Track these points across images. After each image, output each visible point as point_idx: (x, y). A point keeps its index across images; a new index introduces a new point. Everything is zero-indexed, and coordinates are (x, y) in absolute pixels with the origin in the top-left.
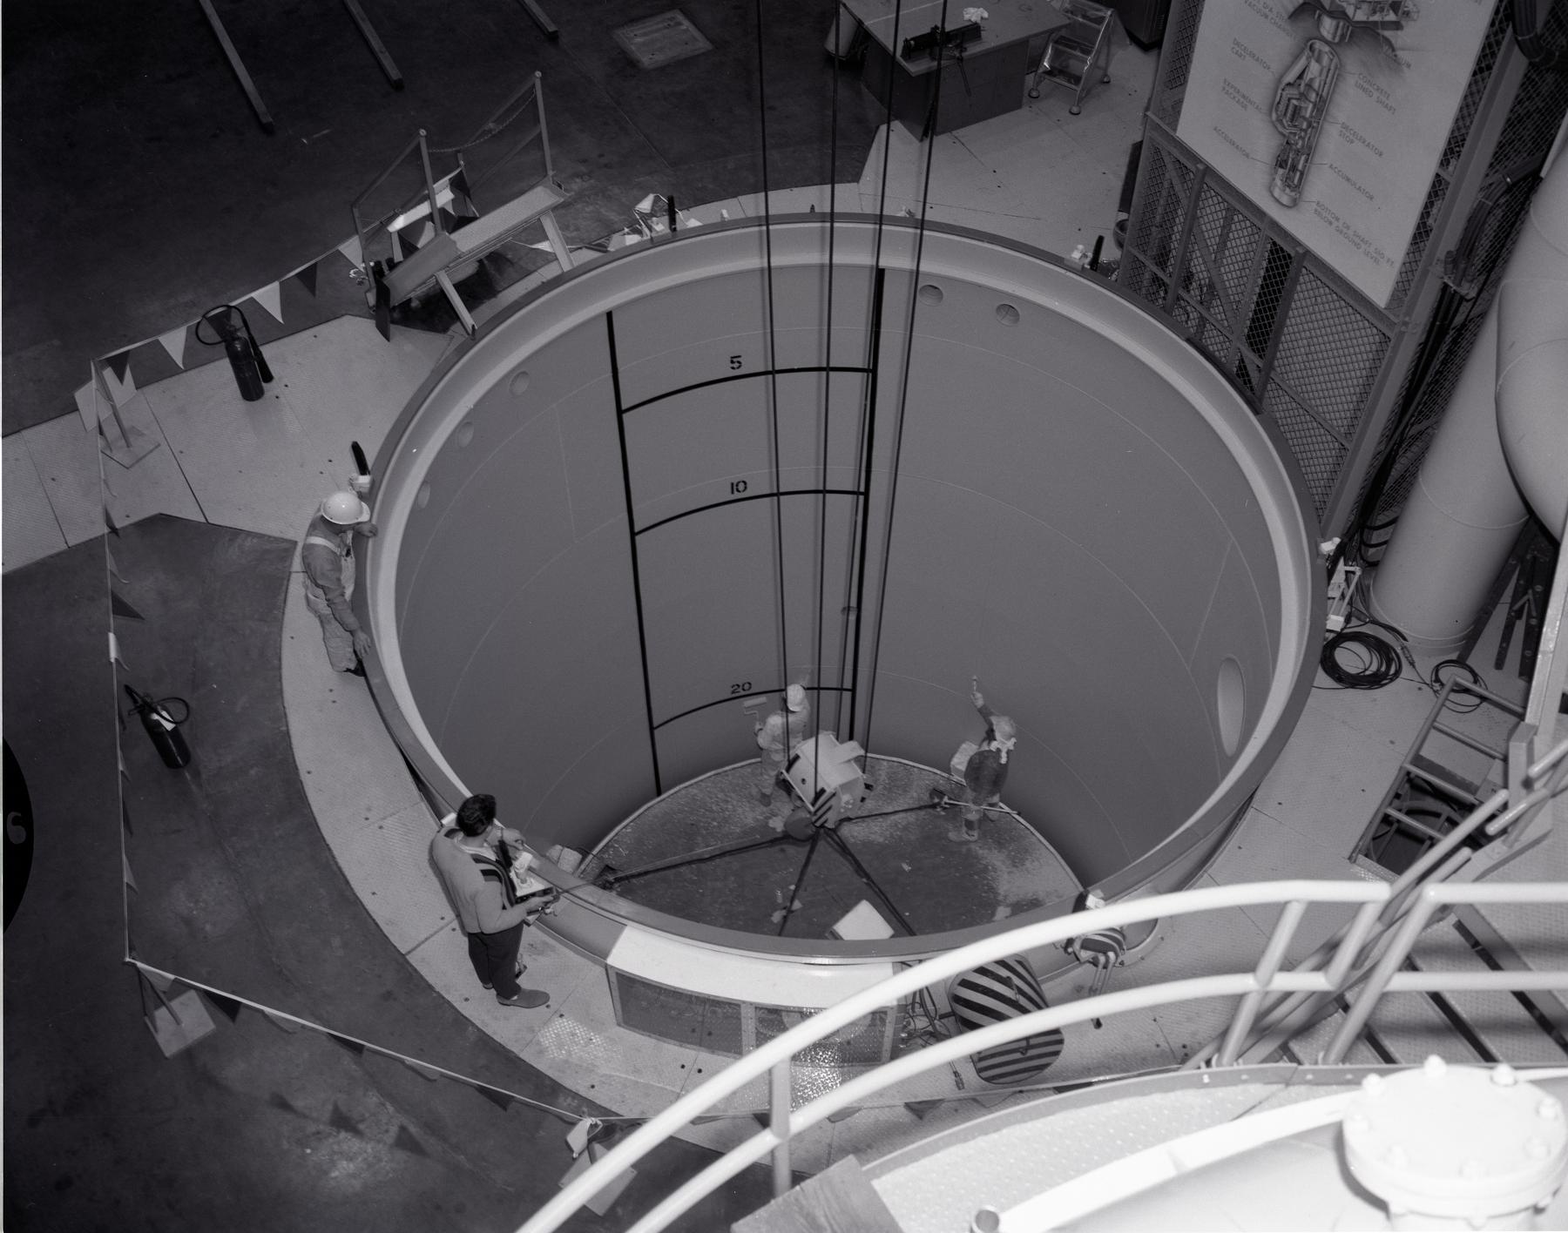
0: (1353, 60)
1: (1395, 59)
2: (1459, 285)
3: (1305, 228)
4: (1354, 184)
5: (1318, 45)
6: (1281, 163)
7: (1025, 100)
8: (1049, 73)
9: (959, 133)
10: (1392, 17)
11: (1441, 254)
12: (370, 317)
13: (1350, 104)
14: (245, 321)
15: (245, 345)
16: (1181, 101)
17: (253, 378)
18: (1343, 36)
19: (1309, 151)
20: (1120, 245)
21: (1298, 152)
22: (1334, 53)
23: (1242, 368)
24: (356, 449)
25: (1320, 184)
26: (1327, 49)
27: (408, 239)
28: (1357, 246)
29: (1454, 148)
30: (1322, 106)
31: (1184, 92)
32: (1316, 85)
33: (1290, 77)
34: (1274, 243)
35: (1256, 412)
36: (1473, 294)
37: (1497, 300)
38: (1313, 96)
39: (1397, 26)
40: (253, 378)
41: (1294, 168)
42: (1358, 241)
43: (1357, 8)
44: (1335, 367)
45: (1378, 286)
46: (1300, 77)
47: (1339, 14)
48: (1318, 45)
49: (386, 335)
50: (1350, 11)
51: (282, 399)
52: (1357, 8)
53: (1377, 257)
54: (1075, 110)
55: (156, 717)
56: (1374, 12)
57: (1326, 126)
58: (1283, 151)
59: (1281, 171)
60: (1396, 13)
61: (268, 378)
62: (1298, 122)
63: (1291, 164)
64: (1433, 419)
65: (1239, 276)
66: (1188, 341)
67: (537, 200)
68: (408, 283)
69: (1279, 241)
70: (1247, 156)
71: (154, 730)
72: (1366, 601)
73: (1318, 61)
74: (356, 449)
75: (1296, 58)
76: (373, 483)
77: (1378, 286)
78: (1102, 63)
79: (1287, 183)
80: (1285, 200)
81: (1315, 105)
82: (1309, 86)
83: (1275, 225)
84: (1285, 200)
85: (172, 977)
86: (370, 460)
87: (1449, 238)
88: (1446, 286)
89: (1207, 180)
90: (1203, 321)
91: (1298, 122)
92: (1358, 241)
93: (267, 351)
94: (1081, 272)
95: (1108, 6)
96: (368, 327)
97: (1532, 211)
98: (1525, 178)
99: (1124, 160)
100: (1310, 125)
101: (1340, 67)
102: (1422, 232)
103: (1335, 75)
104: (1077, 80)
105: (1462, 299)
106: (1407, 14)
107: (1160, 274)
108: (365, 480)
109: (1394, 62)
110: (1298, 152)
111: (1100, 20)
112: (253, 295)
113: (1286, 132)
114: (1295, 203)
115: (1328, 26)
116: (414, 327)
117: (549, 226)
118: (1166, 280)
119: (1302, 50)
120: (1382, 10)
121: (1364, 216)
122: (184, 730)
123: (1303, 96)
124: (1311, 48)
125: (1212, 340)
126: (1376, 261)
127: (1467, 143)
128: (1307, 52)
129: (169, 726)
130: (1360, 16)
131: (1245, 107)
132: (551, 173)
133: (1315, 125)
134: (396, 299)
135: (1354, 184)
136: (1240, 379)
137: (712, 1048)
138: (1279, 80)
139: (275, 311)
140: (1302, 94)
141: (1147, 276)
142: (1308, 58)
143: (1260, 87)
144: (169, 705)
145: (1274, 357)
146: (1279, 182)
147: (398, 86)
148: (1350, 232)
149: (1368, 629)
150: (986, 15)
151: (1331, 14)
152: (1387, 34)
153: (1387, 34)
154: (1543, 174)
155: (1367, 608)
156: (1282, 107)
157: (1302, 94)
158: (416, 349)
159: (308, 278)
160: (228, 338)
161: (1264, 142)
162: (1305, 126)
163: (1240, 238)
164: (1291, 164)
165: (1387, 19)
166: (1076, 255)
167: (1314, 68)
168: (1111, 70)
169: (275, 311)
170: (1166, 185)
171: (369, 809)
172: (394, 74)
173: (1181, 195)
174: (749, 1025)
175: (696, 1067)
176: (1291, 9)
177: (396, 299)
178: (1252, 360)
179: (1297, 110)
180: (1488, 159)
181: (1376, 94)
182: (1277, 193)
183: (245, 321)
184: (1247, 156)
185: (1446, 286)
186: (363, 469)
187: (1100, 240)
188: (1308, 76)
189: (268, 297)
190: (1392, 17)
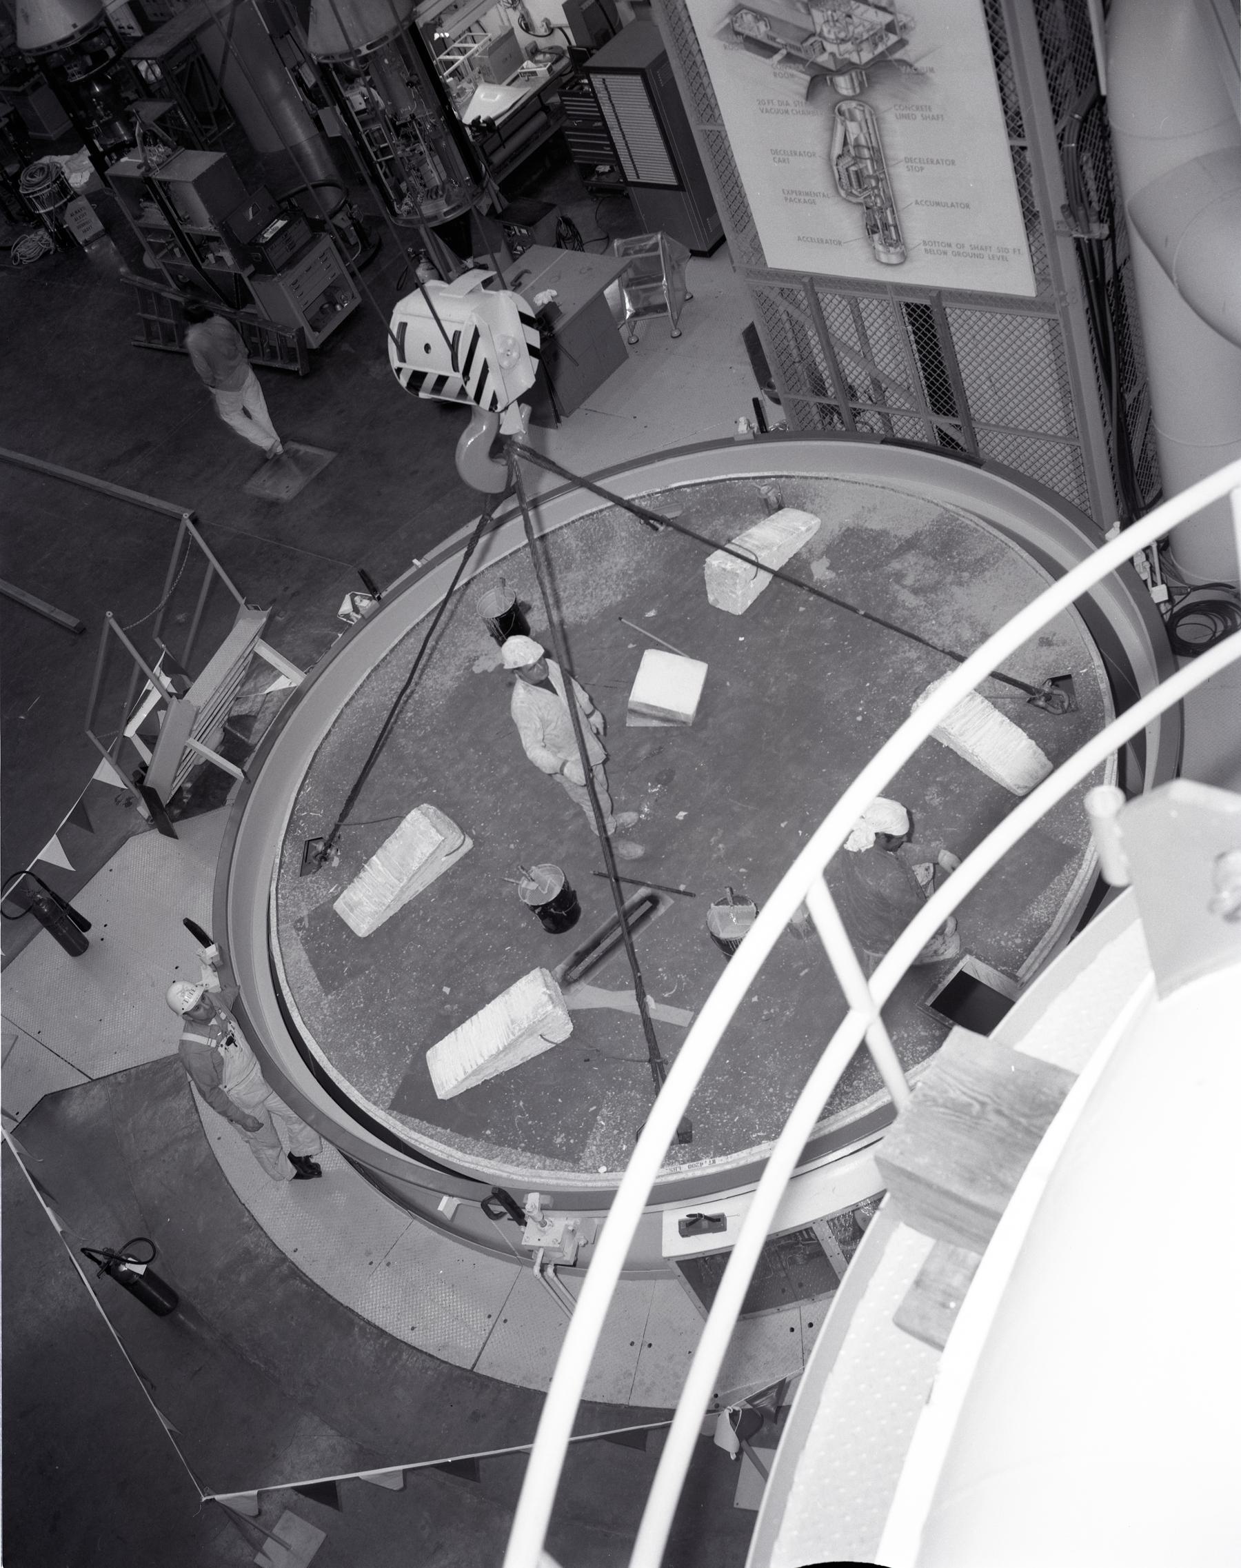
0: (883, 99)
1: (918, 73)
2: (1089, 232)
3: (925, 272)
4: (946, 205)
5: (844, 106)
6: (872, 230)
7: (628, 347)
8: (636, 315)
9: (589, 403)
10: (893, 39)
11: (1057, 215)
12: (152, 827)
13: (901, 138)
14: (39, 881)
15: (49, 902)
16: (756, 236)
17: (73, 933)
18: (861, 84)
19: (890, 202)
20: (777, 401)
21: (881, 210)
22: (862, 103)
23: (944, 436)
24: (190, 925)
25: (917, 225)
26: (854, 104)
27: (149, 735)
28: (978, 256)
29: (1015, 124)
30: (878, 156)
31: (754, 226)
32: (863, 142)
33: (837, 150)
34: (907, 305)
35: (978, 464)
36: (1106, 231)
37: (1128, 217)
38: (866, 153)
39: (902, 43)
40: (73, 933)
41: (886, 226)
42: (978, 253)
43: (859, 52)
44: (1025, 378)
45: (1019, 280)
46: (845, 143)
47: (846, 67)
48: (844, 106)
49: (170, 833)
50: (855, 58)
51: (106, 937)
52: (859, 52)
53: (1002, 256)
54: (676, 333)
55: (123, 1268)
56: (876, 45)
57: (892, 170)
58: (868, 217)
59: (876, 237)
60: (895, 33)
61: (86, 925)
62: (864, 181)
63: (882, 225)
64: (1140, 382)
65: (893, 355)
66: (884, 442)
67: (245, 632)
68: (166, 776)
69: (910, 300)
70: (840, 243)
71: (128, 1281)
72: (1178, 577)
73: (853, 119)
74: (190, 925)
75: (832, 130)
76: (220, 949)
77: (1019, 280)
78: (678, 285)
79: (888, 243)
80: (894, 259)
81: (872, 159)
82: (857, 146)
83: (900, 289)
84: (894, 259)
85: (255, 1492)
86: (209, 931)
87: (1052, 191)
88: (1078, 240)
89: (817, 289)
90: (886, 419)
91: (864, 181)
92: (978, 253)
93: (77, 904)
94: (756, 439)
95: (656, 232)
96: (154, 838)
97: (1112, 123)
98: (1092, 106)
99: (742, 349)
100: (878, 180)
101: (874, 111)
102: (1030, 217)
103: (875, 122)
104: (663, 307)
105: (1100, 242)
106: (904, 27)
107: (825, 401)
108: (212, 951)
109: (920, 76)
110: (881, 210)
111: (655, 247)
112: (39, 857)
113: (861, 200)
114: (904, 257)
115: (844, 84)
116: (193, 815)
117: (267, 653)
118: (833, 403)
119: (834, 120)
120: (881, 38)
121: (969, 222)
122: (156, 1267)
123: (858, 158)
124: (841, 113)
125: (903, 428)
126: (1004, 259)
127: (1023, 115)
128: (839, 119)
129: (140, 1269)
130: (866, 56)
131: (814, 202)
132: (242, 601)
133: (882, 177)
134: (165, 799)
135: (946, 205)
136: (947, 446)
137: (810, 1296)
138: (830, 159)
139: (65, 863)
140: (855, 158)
141: (814, 410)
142: (843, 123)
143: (816, 176)
144: (130, 1250)
145: (967, 408)
146: (880, 248)
147: (81, 631)
148: (967, 249)
149: (1194, 598)
150: (554, 293)
151: (840, 72)
152: (898, 55)
153: (898, 55)
154: (1104, 92)
155: (1183, 582)
156: (845, 181)
157: (855, 158)
158: (206, 827)
159: (81, 818)
160: (31, 908)
161: (845, 220)
162: (874, 184)
163: (869, 305)
164: (882, 225)
165: (890, 43)
166: (743, 428)
167: (853, 128)
168: (689, 289)
169: (65, 863)
170: (785, 317)
171: (368, 1253)
172: (71, 621)
173: (802, 318)
174: (831, 1246)
175: (805, 1324)
176: (804, 91)
177: (165, 799)
178: (945, 422)
179: (858, 174)
180: (1047, 107)
181: (918, 114)
182: (884, 258)
183: (39, 881)
184: (840, 243)
185: (1078, 240)
186: (205, 941)
187: (756, 402)
188: (851, 139)
189: (53, 853)
190: (893, 39)
